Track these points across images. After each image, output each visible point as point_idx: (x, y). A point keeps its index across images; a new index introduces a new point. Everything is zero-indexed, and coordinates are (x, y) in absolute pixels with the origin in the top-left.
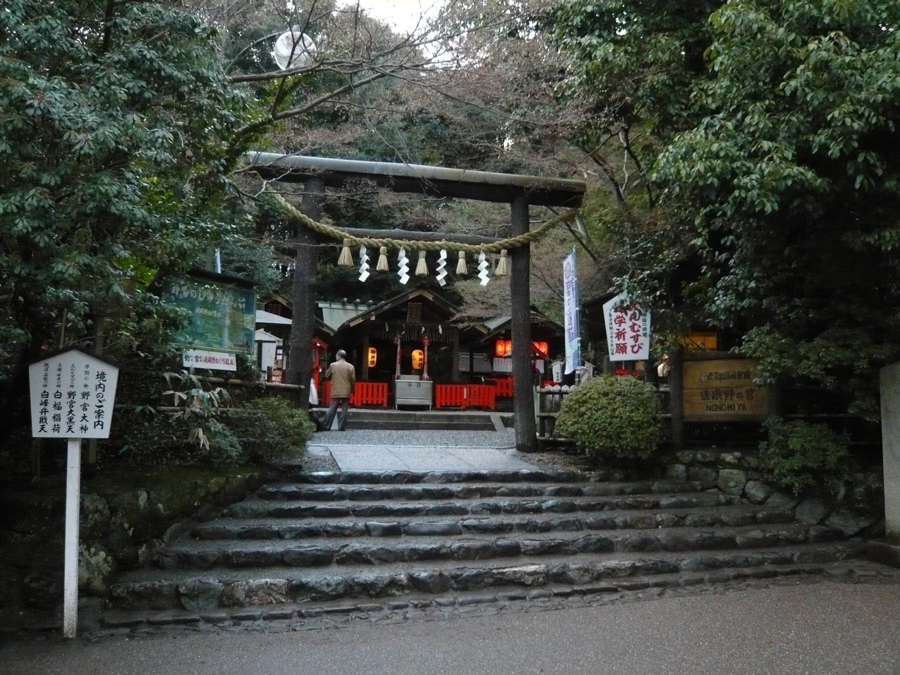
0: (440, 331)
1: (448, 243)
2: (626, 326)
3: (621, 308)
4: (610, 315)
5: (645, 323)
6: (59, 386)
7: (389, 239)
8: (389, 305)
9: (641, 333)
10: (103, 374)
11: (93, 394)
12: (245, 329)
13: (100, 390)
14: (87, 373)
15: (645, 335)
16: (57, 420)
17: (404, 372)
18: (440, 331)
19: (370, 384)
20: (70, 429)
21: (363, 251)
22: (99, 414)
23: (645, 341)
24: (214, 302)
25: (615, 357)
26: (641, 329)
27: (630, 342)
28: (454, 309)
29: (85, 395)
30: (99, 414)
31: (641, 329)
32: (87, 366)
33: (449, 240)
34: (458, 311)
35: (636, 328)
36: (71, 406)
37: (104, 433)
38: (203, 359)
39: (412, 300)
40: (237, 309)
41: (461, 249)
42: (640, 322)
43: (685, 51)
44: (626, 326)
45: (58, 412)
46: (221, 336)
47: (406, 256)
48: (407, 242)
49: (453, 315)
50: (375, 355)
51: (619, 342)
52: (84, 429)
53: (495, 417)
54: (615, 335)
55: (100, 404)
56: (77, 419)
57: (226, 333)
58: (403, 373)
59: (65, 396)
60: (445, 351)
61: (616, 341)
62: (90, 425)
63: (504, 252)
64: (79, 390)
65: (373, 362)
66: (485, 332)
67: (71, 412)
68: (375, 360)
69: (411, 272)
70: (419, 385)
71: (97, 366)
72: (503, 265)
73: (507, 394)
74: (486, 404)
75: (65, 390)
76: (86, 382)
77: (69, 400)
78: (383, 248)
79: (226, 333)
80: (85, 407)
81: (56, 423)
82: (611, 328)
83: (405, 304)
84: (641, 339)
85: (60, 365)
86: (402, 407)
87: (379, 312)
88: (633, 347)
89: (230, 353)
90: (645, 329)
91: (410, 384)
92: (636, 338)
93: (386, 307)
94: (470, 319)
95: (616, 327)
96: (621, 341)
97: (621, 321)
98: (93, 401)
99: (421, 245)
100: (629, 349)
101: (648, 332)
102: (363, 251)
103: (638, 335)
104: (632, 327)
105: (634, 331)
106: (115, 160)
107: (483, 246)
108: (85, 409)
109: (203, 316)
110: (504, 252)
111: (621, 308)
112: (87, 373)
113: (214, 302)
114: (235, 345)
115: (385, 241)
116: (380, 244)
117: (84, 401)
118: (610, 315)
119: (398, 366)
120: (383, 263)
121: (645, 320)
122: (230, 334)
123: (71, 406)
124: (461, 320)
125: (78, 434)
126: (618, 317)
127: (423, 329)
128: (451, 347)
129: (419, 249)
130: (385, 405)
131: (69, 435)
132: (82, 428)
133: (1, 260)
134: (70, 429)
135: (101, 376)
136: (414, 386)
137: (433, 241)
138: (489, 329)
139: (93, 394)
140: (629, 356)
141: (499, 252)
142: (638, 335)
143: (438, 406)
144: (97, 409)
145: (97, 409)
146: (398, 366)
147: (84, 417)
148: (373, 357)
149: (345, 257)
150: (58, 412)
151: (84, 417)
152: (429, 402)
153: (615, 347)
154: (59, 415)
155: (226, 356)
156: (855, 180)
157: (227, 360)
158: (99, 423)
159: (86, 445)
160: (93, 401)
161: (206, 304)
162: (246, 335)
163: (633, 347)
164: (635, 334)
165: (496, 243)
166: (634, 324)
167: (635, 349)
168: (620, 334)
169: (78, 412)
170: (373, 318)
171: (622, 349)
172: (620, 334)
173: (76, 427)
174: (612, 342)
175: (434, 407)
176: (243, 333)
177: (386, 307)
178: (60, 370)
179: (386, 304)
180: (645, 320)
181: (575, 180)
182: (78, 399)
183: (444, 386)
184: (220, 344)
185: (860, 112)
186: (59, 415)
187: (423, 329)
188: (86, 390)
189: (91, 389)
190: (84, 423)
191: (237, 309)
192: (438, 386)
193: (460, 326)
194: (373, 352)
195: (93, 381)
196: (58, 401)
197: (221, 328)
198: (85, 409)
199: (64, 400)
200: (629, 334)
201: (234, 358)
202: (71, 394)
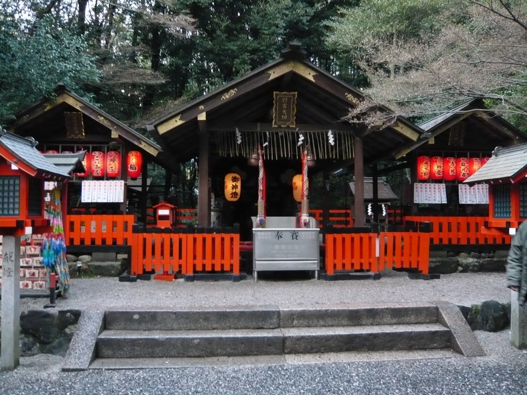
0: (331, 141)
8: (233, 92)
17: (273, 210)
18: (331, 141)
19: (218, 237)
49: (353, 106)
50: (239, 184)
58: (270, 212)
60: (340, 175)
65: (234, 194)
66: (414, 137)
68: (238, 190)
70: (295, 235)
73: (450, 240)
86: (269, 276)
87: (217, 103)
91: (279, 235)
93: (226, 97)
119: (261, 203)
127: (302, 138)
128: (351, 168)
130: (236, 272)
136: (287, 237)
138: (420, 132)
143: (330, 272)
146: (261, 203)
148: (234, 187)
152: (313, 265)
156: (326, 188)
170: (202, 117)
177: (226, 97)
179: (227, 90)
187: (302, 138)
194: (234, 179)
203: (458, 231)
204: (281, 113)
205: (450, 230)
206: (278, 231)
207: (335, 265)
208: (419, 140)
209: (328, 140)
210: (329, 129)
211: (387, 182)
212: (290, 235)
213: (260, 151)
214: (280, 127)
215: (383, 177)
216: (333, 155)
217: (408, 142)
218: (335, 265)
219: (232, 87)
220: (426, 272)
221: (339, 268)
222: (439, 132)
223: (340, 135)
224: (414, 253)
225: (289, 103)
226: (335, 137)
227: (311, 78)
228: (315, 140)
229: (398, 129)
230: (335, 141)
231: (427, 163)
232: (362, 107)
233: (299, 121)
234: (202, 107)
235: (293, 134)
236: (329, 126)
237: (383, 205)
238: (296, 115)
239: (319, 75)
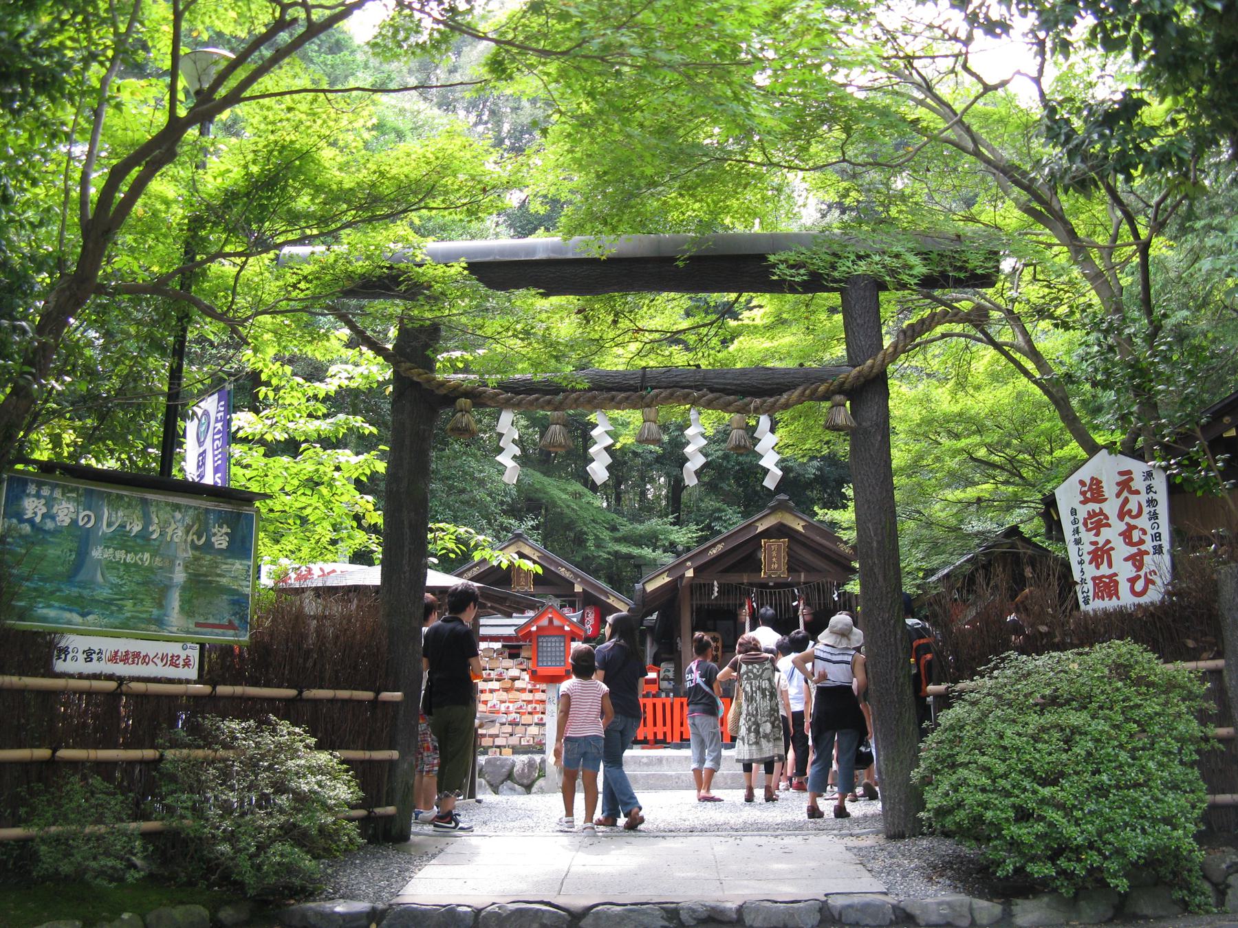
2: (1112, 533)
4: (1074, 512)
9: (1149, 545)
24: (144, 535)
26: (1148, 538)
27: (1124, 570)
31: (1148, 538)
35: (1136, 536)
39: (767, 534)
42: (1143, 522)
43: (66, 323)
44: (1112, 533)
46: (160, 606)
51: (1098, 573)
54: (1087, 558)
57: (175, 600)
61: (1091, 571)
79: (175, 600)
88: (1133, 581)
90: (1157, 537)
92: (1136, 560)
95: (1087, 537)
96: (1104, 570)
100: (1124, 588)
103: (1143, 553)
104: (1127, 535)
105: (1130, 543)
109: (112, 565)
113: (144, 535)
122: (184, 602)
126: (1092, 515)
133: (158, 11)
142: (1143, 553)
153: (1090, 585)
155: (174, 649)
161: (121, 539)
162: (234, 603)
163: (1133, 581)
164: (1134, 550)
166: (1131, 528)
167: (1139, 586)
170: (690, 573)
172: (1101, 554)
177: (714, 552)
179: (714, 546)
184: (160, 622)
185: (1078, 160)
197: (165, 589)
200: (1121, 550)
201: (194, 654)
219: (719, 542)
234: (689, 564)
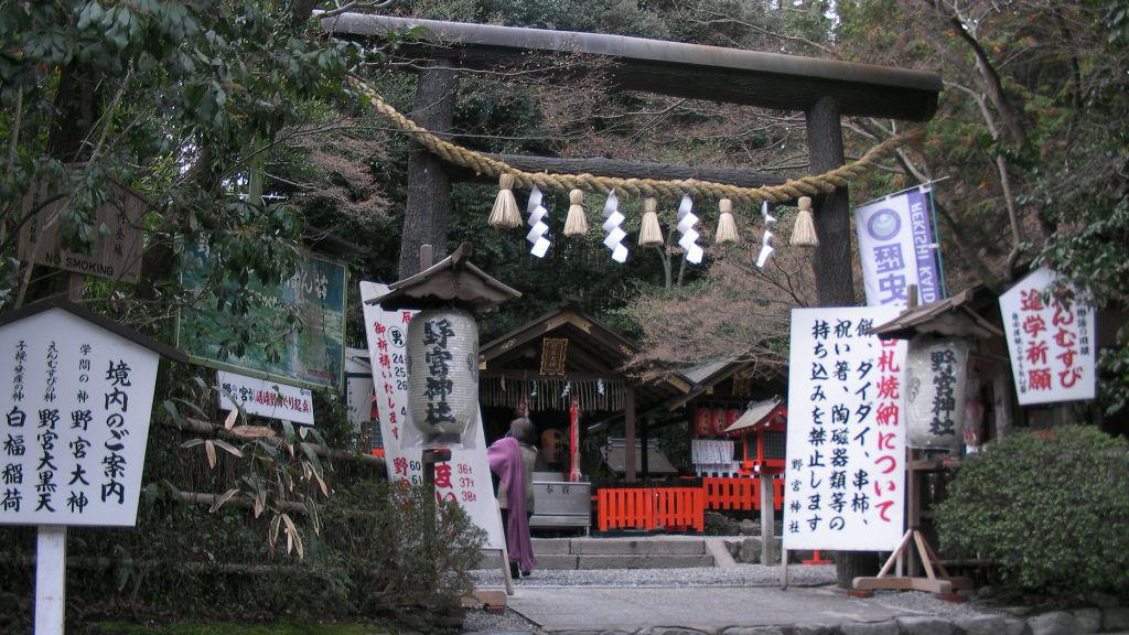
0: (601, 390)
1: (698, 183)
3: (1034, 301)
5: (1083, 328)
6: (19, 396)
7: (587, 175)
8: (512, 342)
10: (123, 366)
11: (100, 415)
12: (327, 340)
13: (116, 408)
14: (85, 364)
15: (1085, 351)
16: (13, 480)
18: (601, 390)
20: (44, 502)
21: (536, 198)
22: (114, 465)
23: (1087, 364)
25: (1027, 397)
26: (1077, 341)
27: (1055, 366)
28: (629, 347)
29: (81, 418)
30: (114, 465)
31: (1077, 341)
32: (86, 349)
33: (701, 177)
34: (636, 351)
35: (1067, 338)
36: (47, 445)
37: (124, 514)
38: (255, 395)
40: (312, 296)
41: (725, 194)
42: (1074, 328)
44: (1048, 336)
45: (15, 460)
47: (620, 209)
48: (620, 181)
49: (628, 359)
51: (1034, 368)
52: (78, 502)
53: (715, 544)
54: (1025, 355)
55: (115, 441)
56: (62, 477)
59: (33, 420)
61: (1028, 366)
62: (93, 493)
63: (804, 201)
64: (66, 405)
66: (686, 389)
67: (46, 459)
69: (630, 240)
71: (108, 349)
72: (804, 228)
74: (689, 523)
75: (32, 405)
76: (83, 387)
77: (43, 430)
78: (575, 194)
80: (79, 448)
81: (12, 487)
82: (1018, 341)
83: (536, 344)
84: (1078, 360)
85: (22, 345)
87: (497, 353)
88: (1063, 375)
89: (302, 386)
90: (1085, 340)
92: (1067, 358)
94: (658, 364)
95: (1026, 337)
96: (1039, 365)
97: (1035, 326)
98: (98, 433)
99: (647, 187)
100: (1055, 380)
101: (1091, 345)
102: (536, 198)
103: (1071, 353)
105: (1062, 344)
106: (48, 53)
107: (766, 190)
108: (79, 453)
110: (804, 201)
111: (1034, 301)
112: (85, 364)
114: (310, 371)
115: (580, 178)
116: (570, 185)
117: (79, 432)
118: (1015, 317)
120: (575, 221)
121: (1083, 324)
123: (47, 445)
124: (643, 369)
125: (65, 515)
126: (1030, 320)
129: (644, 194)
131: (44, 517)
132: (73, 500)
134: (44, 502)
135: (119, 372)
137: (670, 178)
139: (100, 415)
140: (1055, 393)
141: (793, 202)
143: (603, 528)
144: (109, 454)
145: (109, 454)
147: (78, 473)
149: (504, 208)
150: (15, 460)
151: (78, 473)
152: (586, 522)
153: (1027, 377)
154: (18, 468)
157: (298, 401)
158: (113, 489)
159: (82, 541)
160: (98, 433)
163: (1063, 375)
164: (1065, 350)
165: (790, 184)
166: (1063, 332)
167: (1068, 379)
168: (1037, 352)
169: (64, 461)
171: (1041, 380)
172: (1037, 352)
173: (59, 498)
174: (1021, 367)
175: (595, 530)
176: (323, 348)
178: (21, 356)
180: (1083, 324)
181: (921, 68)
182: (65, 430)
183: (612, 492)
186: (18, 468)
188: (83, 407)
189: (95, 404)
190: (78, 487)
191: (312, 296)
192: (603, 492)
193: (647, 376)
195: (100, 386)
196: (15, 432)
198: (79, 453)
199: (31, 431)
200: (1054, 350)
201: (308, 398)
202: (48, 417)
203: (741, 494)
204: (549, 361)
205: (731, 493)
206: (549, 485)
207: (608, 522)
208: (691, 391)
209: (597, 390)
210: (598, 377)
211: (660, 446)
212: (561, 488)
213: (526, 400)
214: (547, 375)
215: (655, 440)
216: (604, 406)
217: (680, 394)
218: (608, 522)
220: (701, 529)
221: (613, 525)
222: (719, 380)
223: (610, 385)
224: (689, 510)
225: (557, 351)
226: (605, 386)
227: (586, 330)
228: (584, 388)
229: (671, 381)
230: (605, 391)
231: (706, 416)
232: (637, 359)
233: (568, 369)
235: (561, 383)
236: (600, 374)
237: (725, 204)
238: (565, 363)
239: (595, 327)
